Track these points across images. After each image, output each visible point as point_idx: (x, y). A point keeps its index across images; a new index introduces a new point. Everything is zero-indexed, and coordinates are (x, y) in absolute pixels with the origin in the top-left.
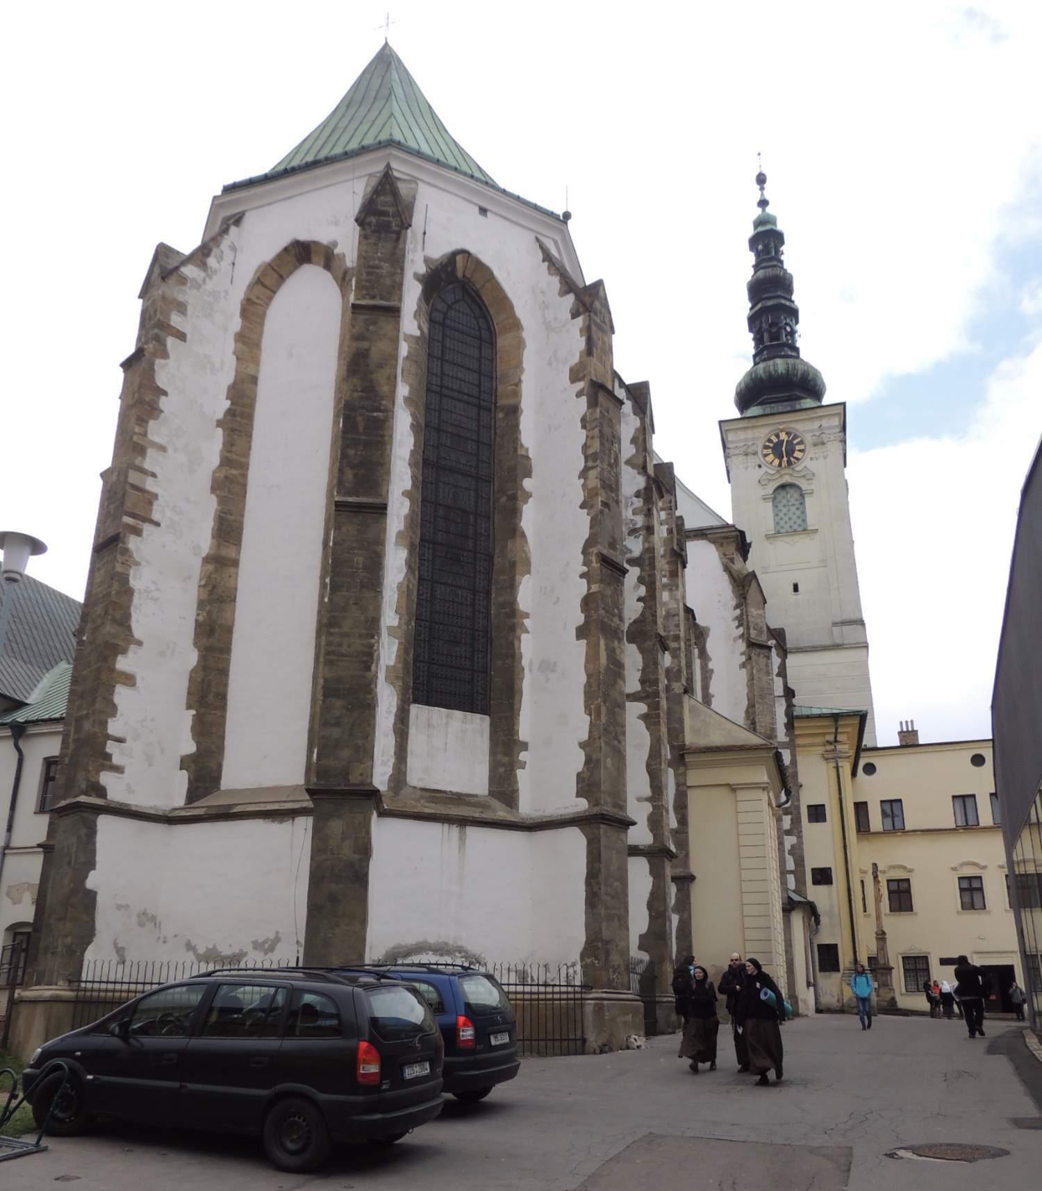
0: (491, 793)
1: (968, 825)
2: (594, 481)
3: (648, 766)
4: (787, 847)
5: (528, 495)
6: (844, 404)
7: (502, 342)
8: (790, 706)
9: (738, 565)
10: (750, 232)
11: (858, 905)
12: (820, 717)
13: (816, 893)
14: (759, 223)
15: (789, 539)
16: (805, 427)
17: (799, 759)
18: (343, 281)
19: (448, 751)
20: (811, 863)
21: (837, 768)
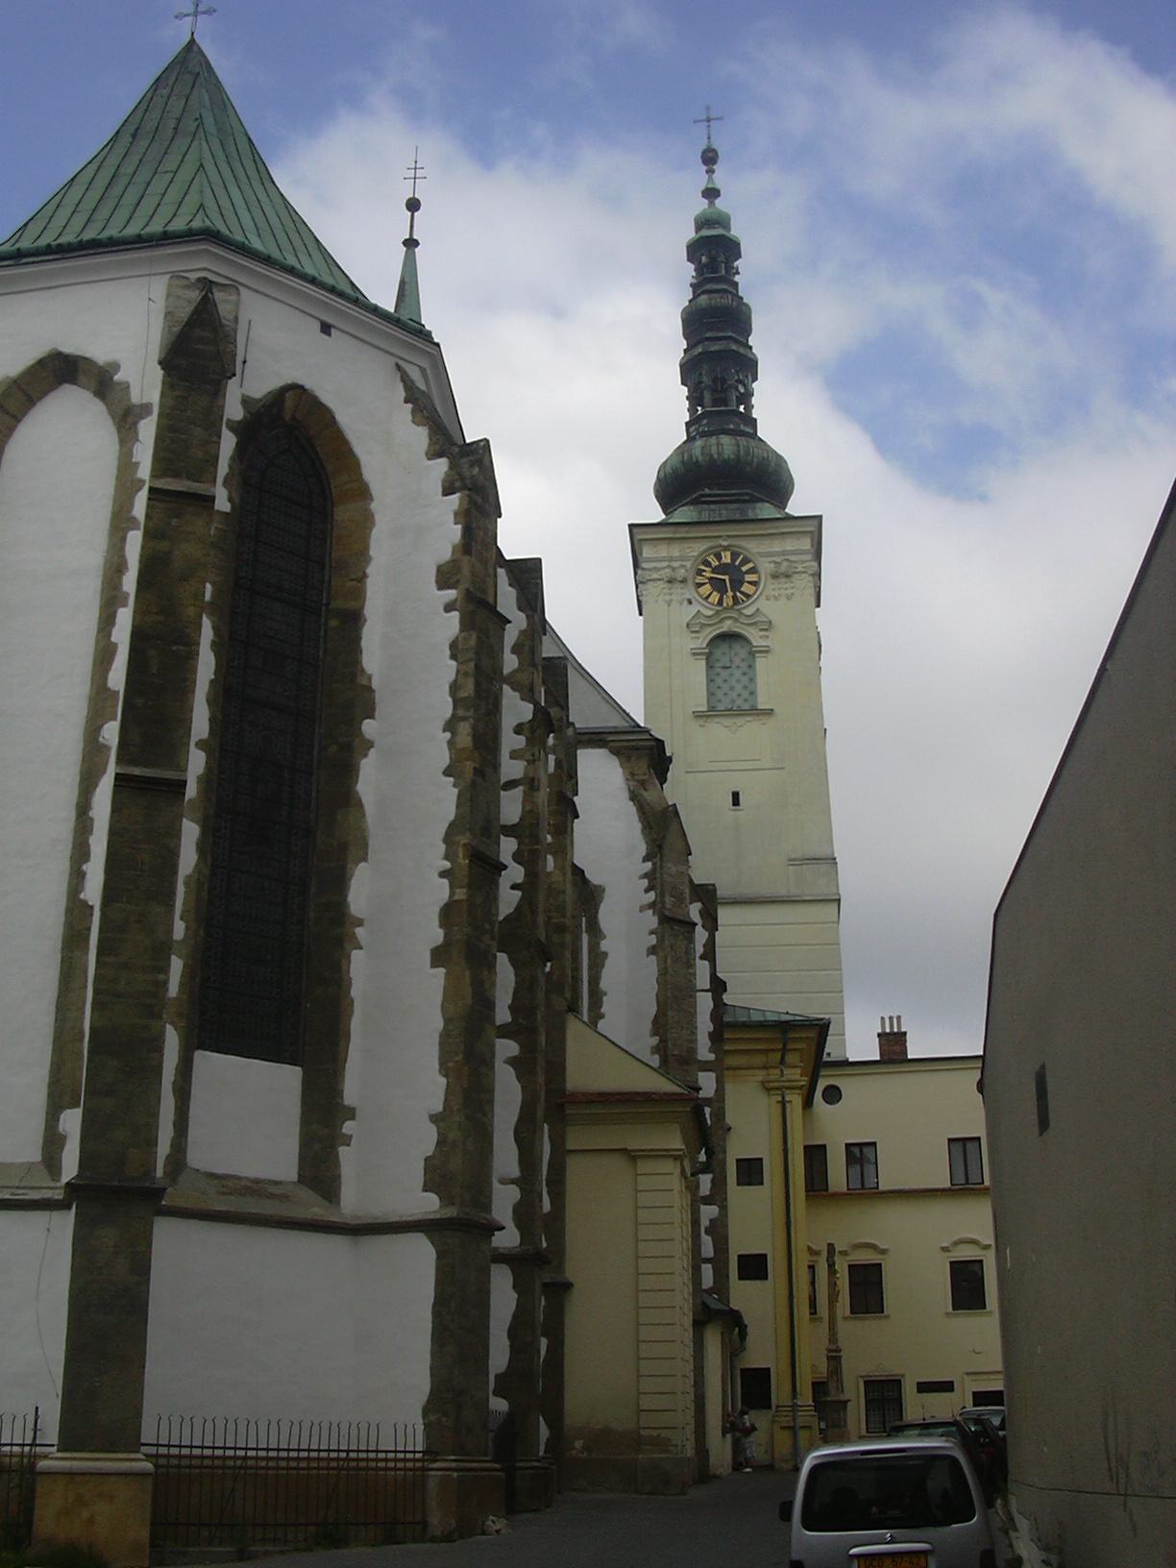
0: (302, 1179)
1: (964, 1187)
2: (465, 739)
3: (516, 1132)
4: (705, 1223)
5: (370, 744)
6: (820, 517)
7: (343, 513)
8: (719, 1006)
9: (649, 796)
10: (691, 234)
11: (802, 1308)
12: (763, 1025)
13: (744, 1295)
14: (702, 223)
15: (726, 721)
16: (763, 552)
17: (728, 1087)
18: (126, 419)
19: (238, 1111)
20: (740, 1244)
21: (783, 1103)
